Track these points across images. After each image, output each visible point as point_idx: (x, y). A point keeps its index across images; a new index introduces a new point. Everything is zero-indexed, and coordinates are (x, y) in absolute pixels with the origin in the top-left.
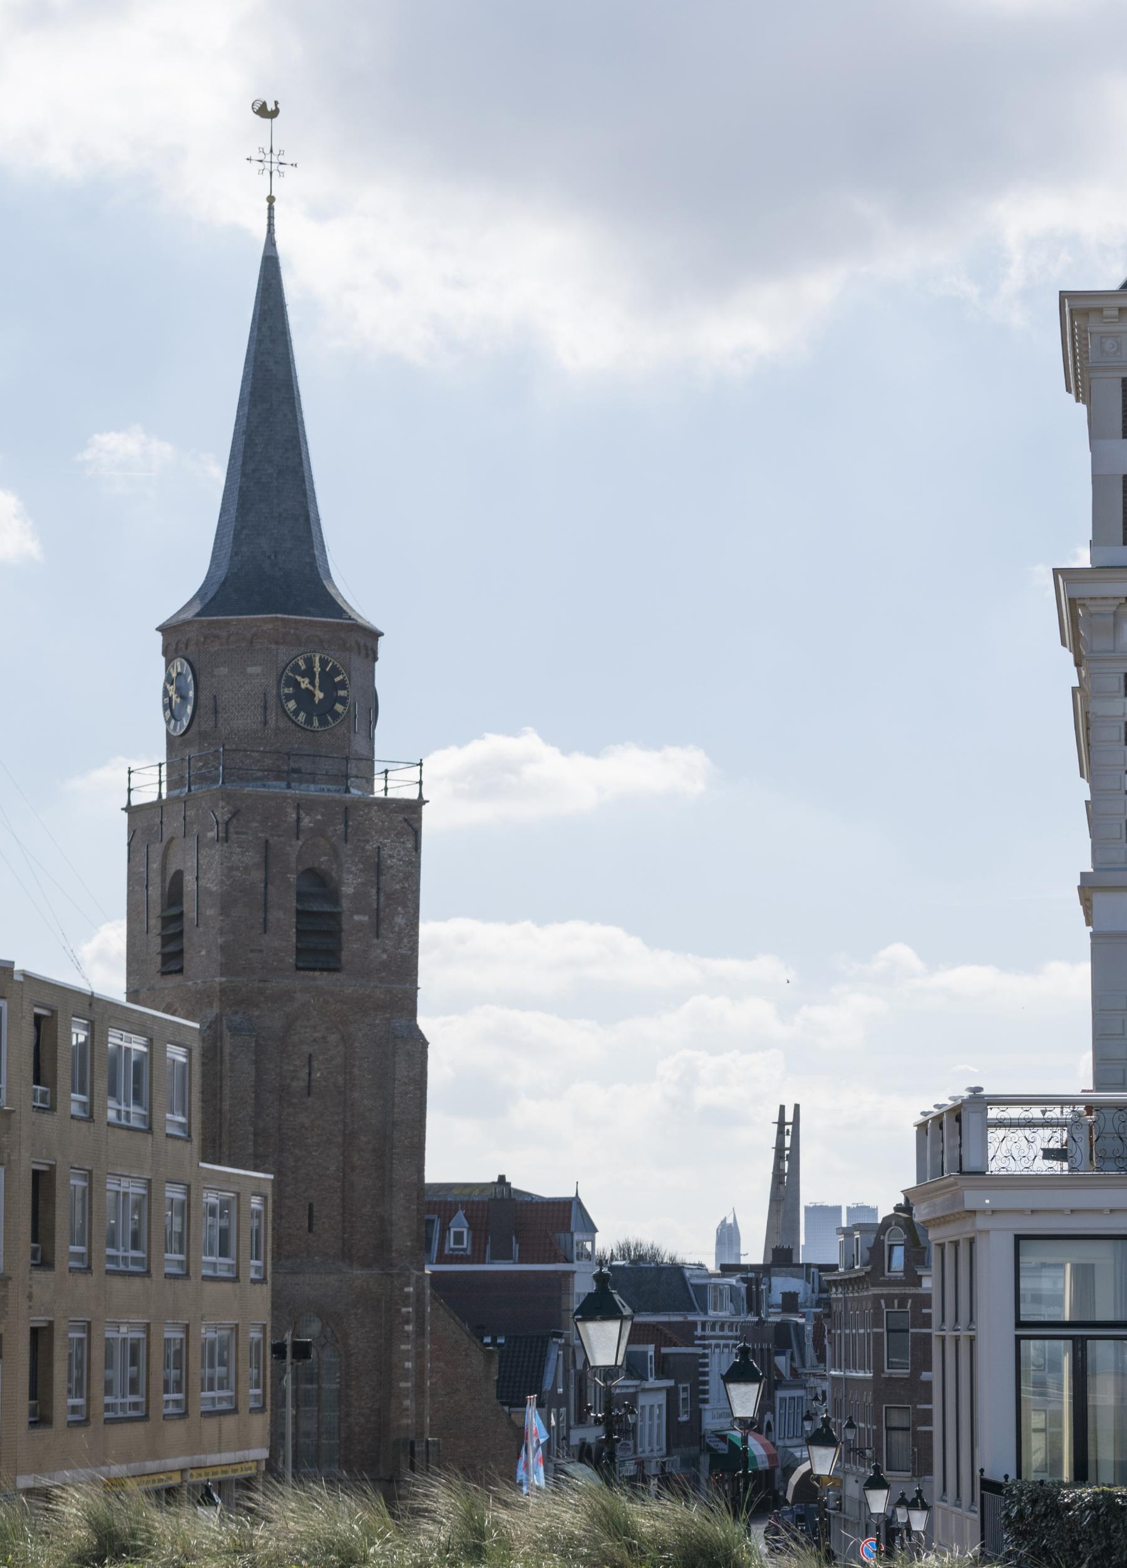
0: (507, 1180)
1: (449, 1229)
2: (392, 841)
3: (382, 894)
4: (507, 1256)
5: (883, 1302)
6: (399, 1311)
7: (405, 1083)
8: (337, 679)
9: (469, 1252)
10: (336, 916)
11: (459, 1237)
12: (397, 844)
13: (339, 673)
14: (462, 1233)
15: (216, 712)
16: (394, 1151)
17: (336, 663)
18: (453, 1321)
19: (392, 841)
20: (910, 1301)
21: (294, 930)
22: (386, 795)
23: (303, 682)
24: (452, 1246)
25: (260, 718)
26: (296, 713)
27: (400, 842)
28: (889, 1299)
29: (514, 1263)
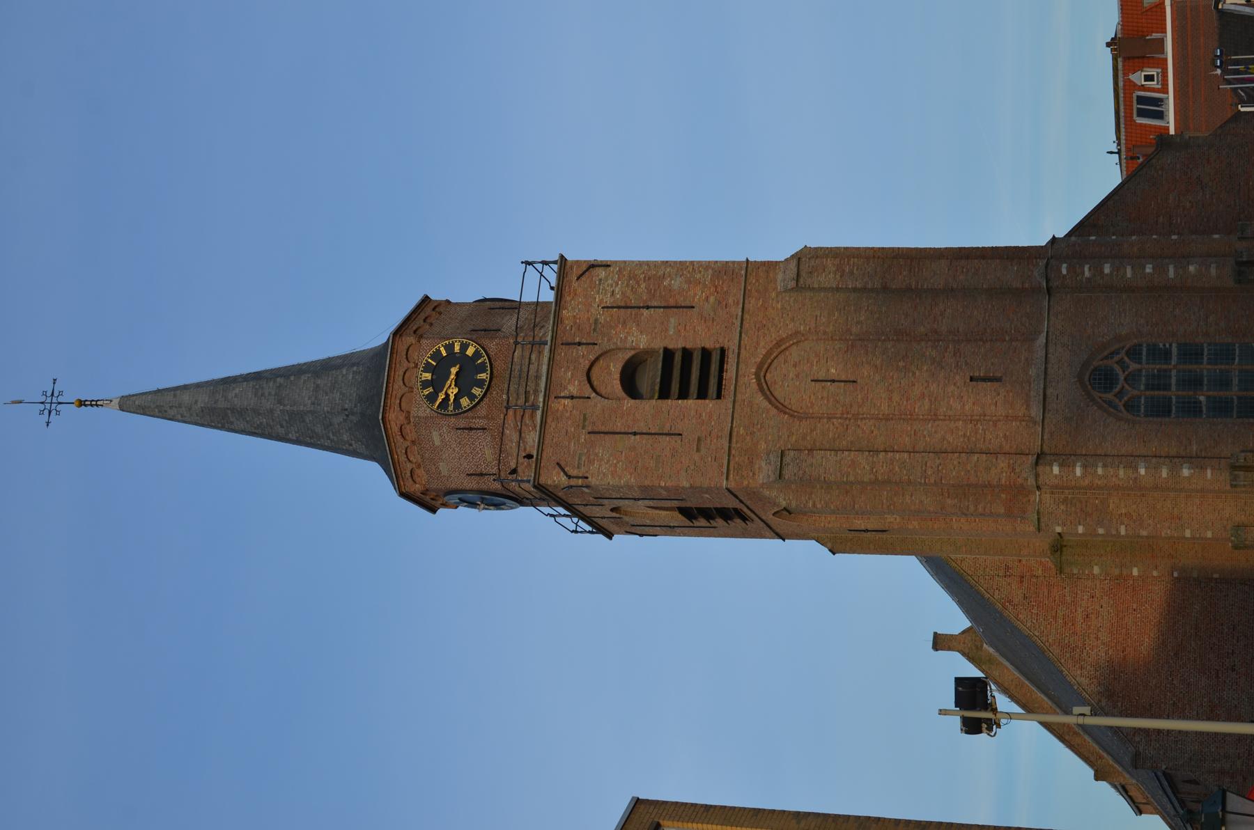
0: (1109, 40)
1: (1143, 85)
2: (598, 293)
3: (650, 304)
4: (1161, 42)
6: (1088, 280)
8: (444, 354)
9: (1160, 70)
10: (668, 354)
11: (1149, 78)
12: (601, 287)
13: (439, 351)
14: (1145, 76)
15: (481, 475)
16: (913, 287)
17: (428, 355)
18: (1126, 185)
19: (598, 293)
21: (680, 401)
24: (1155, 83)
25: (480, 433)
27: (600, 284)
29: (1166, 37)
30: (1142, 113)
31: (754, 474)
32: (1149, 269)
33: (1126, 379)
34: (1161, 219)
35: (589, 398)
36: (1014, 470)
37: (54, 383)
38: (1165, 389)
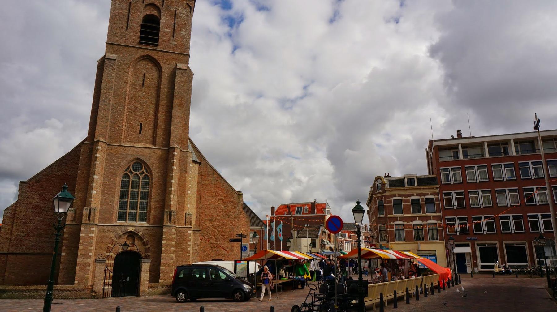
5: (377, 199)
7: (179, 82)
20: (383, 197)
28: (378, 197)
30: (298, 208)
31: (111, 52)
32: (339, 243)
33: (136, 174)
34: (214, 194)
35: (143, 3)
36: (101, 134)
38: (131, 187)
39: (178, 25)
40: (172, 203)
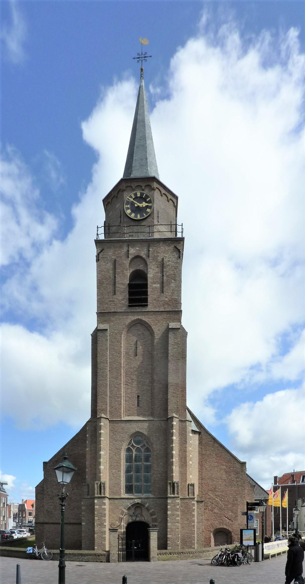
13: (148, 197)
22: (176, 236)
23: (145, 204)
26: (130, 214)
27: (173, 255)
34: (216, 464)
37: (150, 56)
39: (167, 276)
40: (174, 474)
